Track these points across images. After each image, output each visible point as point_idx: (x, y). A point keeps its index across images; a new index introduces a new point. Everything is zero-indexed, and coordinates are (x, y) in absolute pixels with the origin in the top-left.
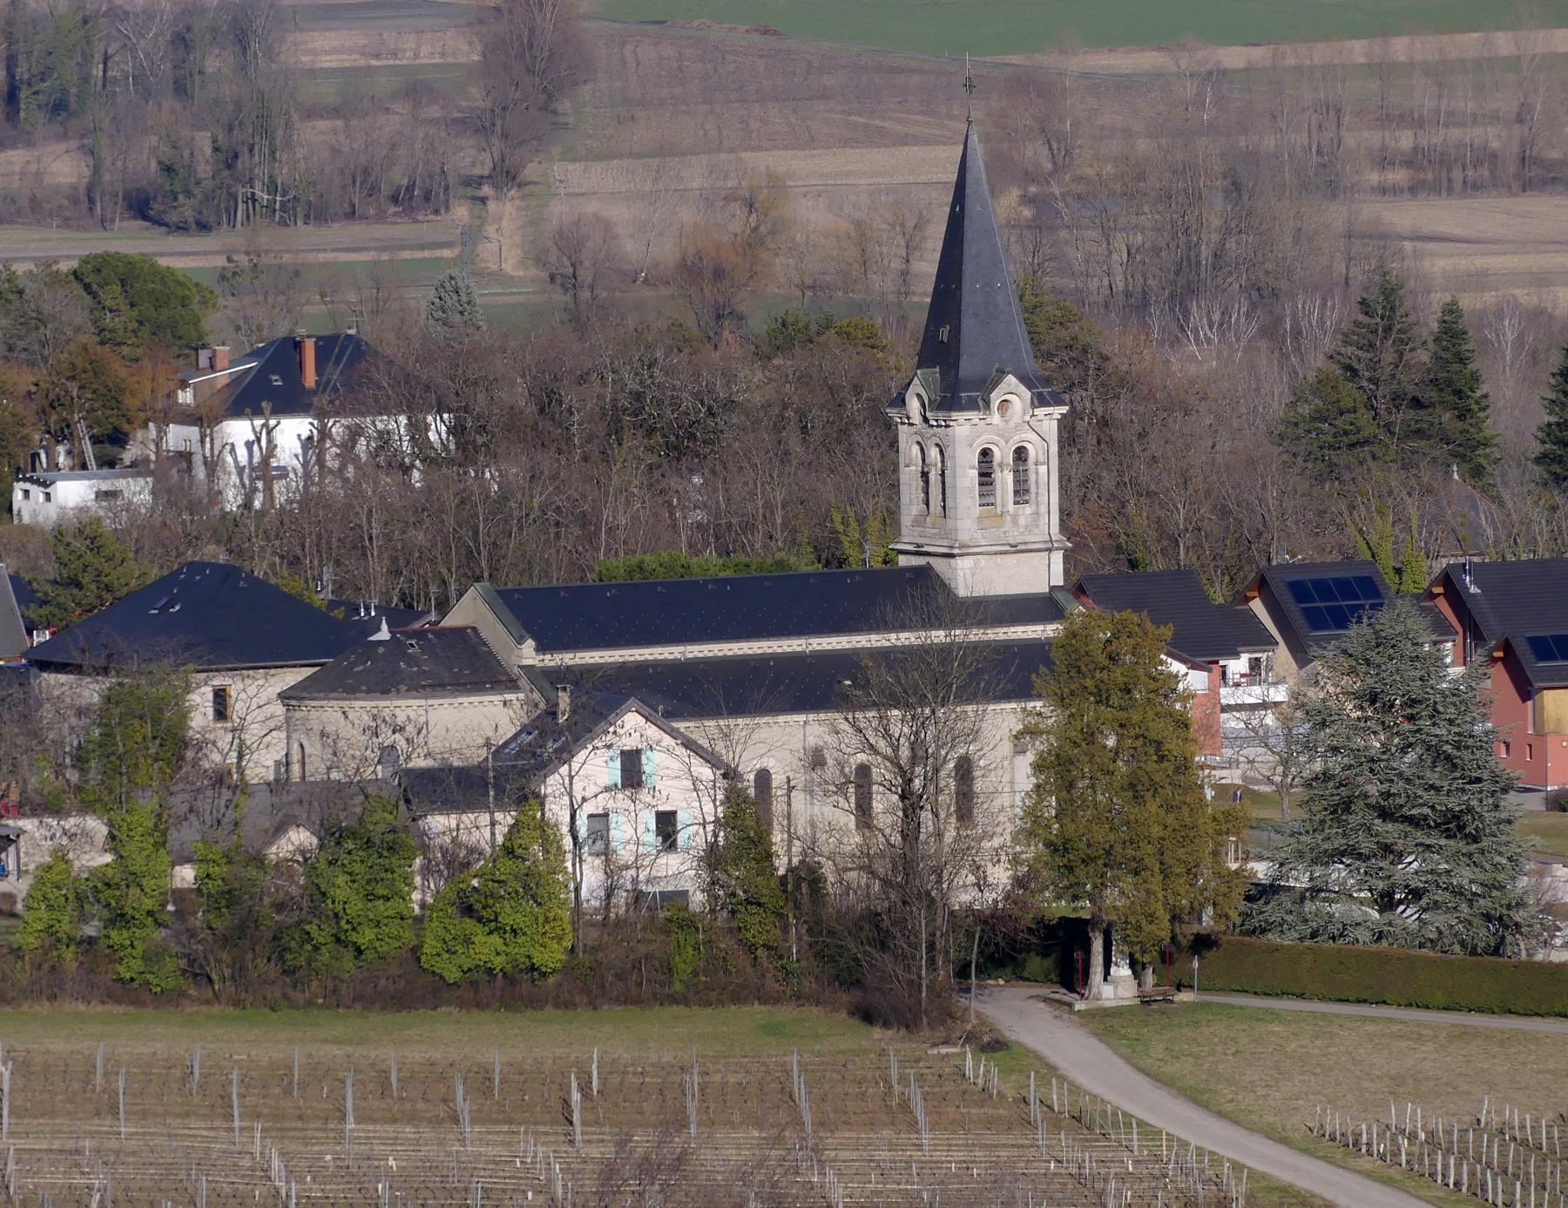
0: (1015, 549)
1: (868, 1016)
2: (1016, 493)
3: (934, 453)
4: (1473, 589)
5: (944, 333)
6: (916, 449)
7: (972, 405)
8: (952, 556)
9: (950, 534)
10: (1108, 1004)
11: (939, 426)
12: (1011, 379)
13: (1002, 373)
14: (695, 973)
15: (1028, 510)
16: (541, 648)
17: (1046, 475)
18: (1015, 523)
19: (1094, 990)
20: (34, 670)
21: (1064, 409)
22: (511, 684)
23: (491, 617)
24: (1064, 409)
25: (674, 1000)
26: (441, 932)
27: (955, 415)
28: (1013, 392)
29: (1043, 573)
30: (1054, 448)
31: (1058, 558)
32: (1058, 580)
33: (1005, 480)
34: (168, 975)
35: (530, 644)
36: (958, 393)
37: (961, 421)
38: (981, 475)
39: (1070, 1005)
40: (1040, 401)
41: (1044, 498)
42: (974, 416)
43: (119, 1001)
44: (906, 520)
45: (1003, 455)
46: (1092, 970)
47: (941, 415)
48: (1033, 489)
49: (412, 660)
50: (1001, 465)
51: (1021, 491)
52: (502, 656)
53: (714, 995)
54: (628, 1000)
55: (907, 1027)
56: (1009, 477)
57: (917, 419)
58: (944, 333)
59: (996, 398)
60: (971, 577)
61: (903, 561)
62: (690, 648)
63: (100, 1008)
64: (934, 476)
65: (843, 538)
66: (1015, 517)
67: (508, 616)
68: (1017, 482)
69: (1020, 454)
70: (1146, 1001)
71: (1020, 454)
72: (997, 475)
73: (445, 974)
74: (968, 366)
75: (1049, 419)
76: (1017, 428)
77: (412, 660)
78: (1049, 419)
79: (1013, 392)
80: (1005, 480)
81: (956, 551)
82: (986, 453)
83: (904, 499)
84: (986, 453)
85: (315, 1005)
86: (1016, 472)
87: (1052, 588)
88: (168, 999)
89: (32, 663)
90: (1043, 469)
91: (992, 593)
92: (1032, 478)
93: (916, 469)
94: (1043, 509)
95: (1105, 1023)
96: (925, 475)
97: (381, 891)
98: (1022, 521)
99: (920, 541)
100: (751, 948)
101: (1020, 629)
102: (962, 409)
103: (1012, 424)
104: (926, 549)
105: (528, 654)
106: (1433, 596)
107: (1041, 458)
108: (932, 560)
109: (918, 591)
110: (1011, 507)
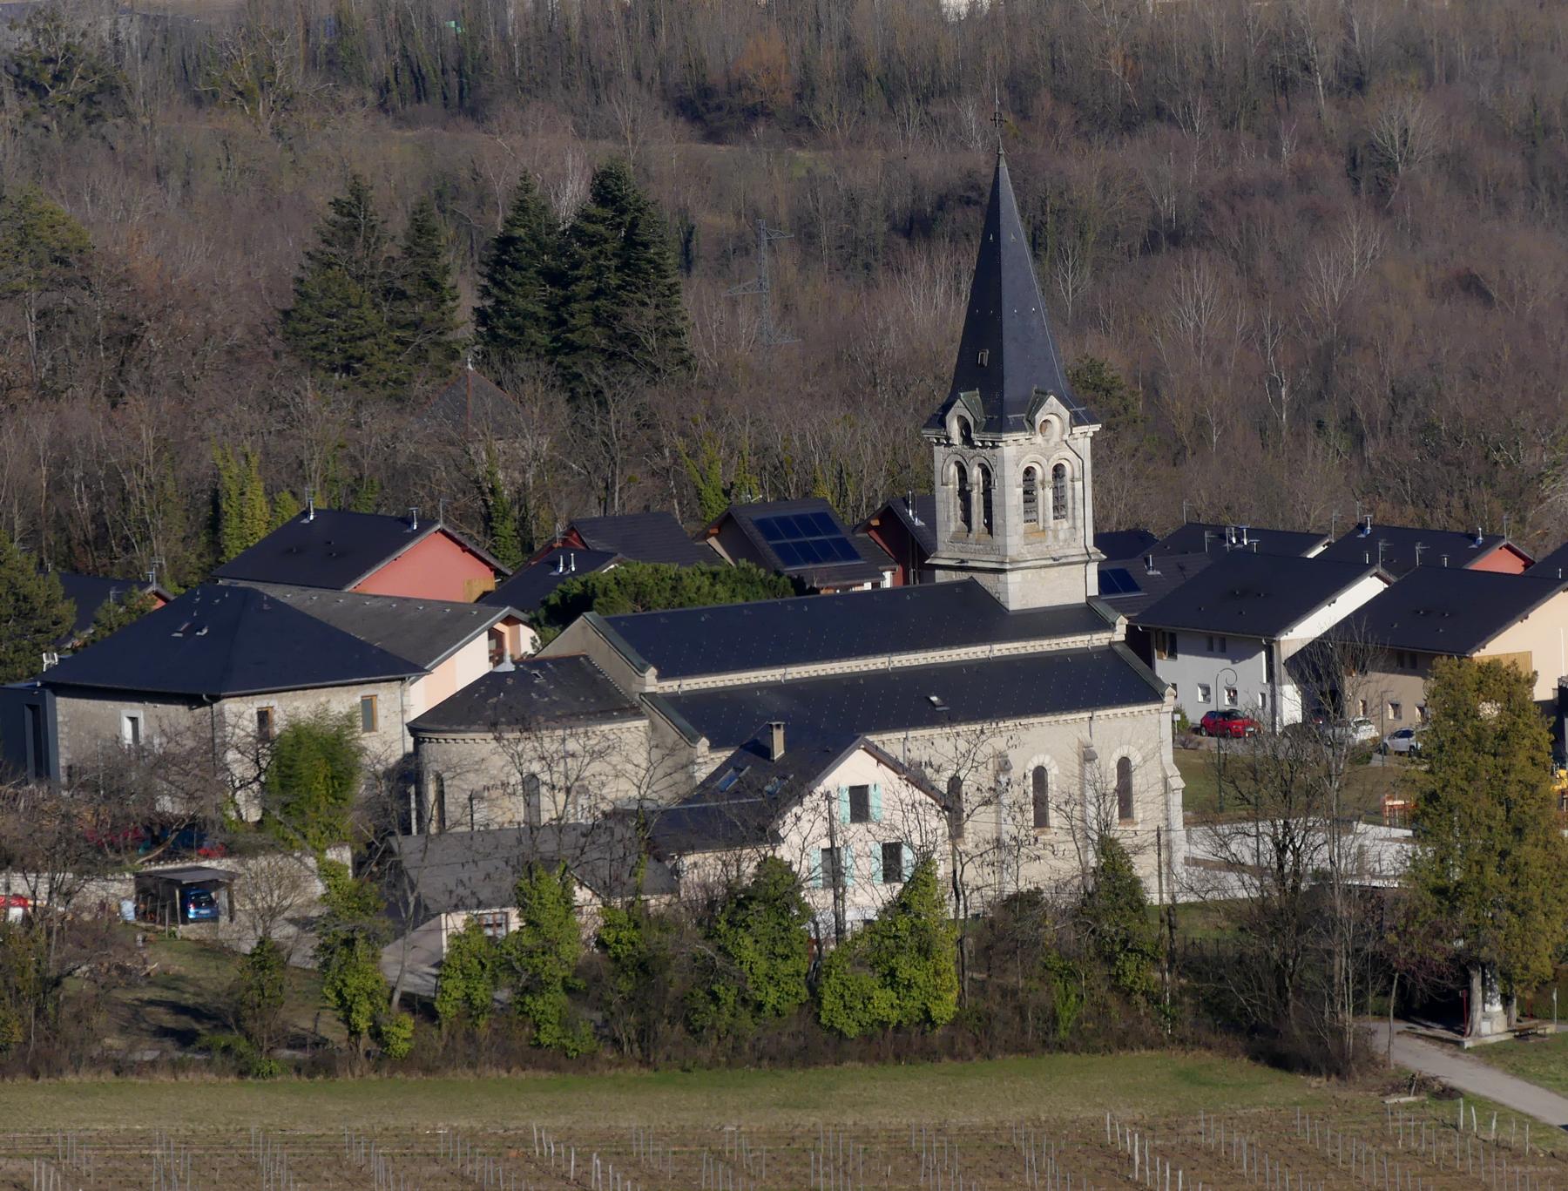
0: (1058, 562)
1: (1281, 1062)
2: (1055, 508)
3: (976, 474)
4: (917, 522)
5: (985, 356)
6: (953, 469)
7: (1019, 427)
8: (1004, 571)
9: (1001, 550)
10: (1492, 1040)
11: (984, 447)
12: (1052, 400)
13: (1041, 397)
14: (1079, 1021)
15: (1065, 524)
16: (661, 676)
17: (1081, 492)
18: (1056, 537)
19: (1476, 1027)
20: (48, 693)
21: (1097, 427)
22: (636, 713)
23: (604, 646)
24: (1097, 427)
25: (1061, 1047)
26: (839, 989)
27: (1005, 436)
28: (1053, 411)
29: (1078, 584)
30: (1088, 465)
31: (1093, 569)
32: (1094, 591)
33: (1046, 496)
34: (584, 1038)
35: (652, 672)
36: (1003, 414)
37: (1010, 441)
38: (1025, 492)
39: (1458, 1044)
40: (1077, 420)
41: (1079, 513)
42: (1021, 436)
43: (536, 1066)
44: (943, 537)
45: (1043, 473)
46: (1474, 1007)
47: (989, 437)
48: (1070, 505)
49: (542, 692)
50: (1043, 483)
51: (1059, 507)
52: (620, 684)
53: (1100, 1042)
54: (1022, 1049)
55: (1338, 1074)
56: (1049, 493)
57: (956, 439)
58: (985, 356)
59: (1040, 417)
60: (1022, 591)
61: (941, 577)
62: (789, 670)
63: (522, 1075)
64: (976, 496)
65: (223, 473)
66: (1056, 531)
67: (625, 646)
68: (1056, 498)
69: (1058, 471)
70: (1523, 1035)
71: (1058, 471)
72: (1040, 493)
73: (845, 1029)
74: (1012, 390)
75: (1084, 435)
76: (1056, 447)
77: (542, 692)
78: (1084, 435)
79: (1053, 411)
80: (1046, 496)
81: (1008, 567)
82: (1029, 472)
83: (941, 516)
84: (1029, 472)
85: (718, 1063)
86: (1055, 488)
87: (1089, 598)
88: (585, 1063)
89: (45, 685)
90: (1078, 485)
91: (1030, 606)
92: (1069, 494)
93: (954, 486)
94: (1079, 523)
95: (1490, 1054)
96: (965, 495)
97: (780, 950)
98: (1062, 536)
99: (963, 556)
100: (1128, 993)
101: (1070, 639)
102: (1011, 430)
103: (1052, 444)
104: (970, 564)
105: (651, 682)
106: (869, 528)
107: (1078, 474)
108: (976, 575)
109: (977, 611)
110: (1051, 522)
